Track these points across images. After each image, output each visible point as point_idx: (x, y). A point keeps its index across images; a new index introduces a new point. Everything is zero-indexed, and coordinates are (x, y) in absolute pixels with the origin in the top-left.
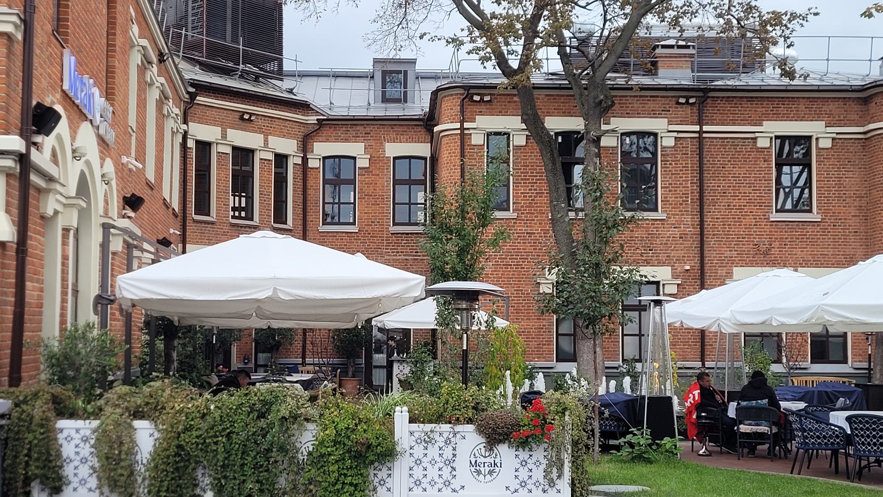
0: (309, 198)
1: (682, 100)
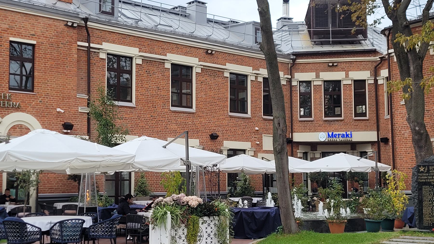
1: (331, 64)
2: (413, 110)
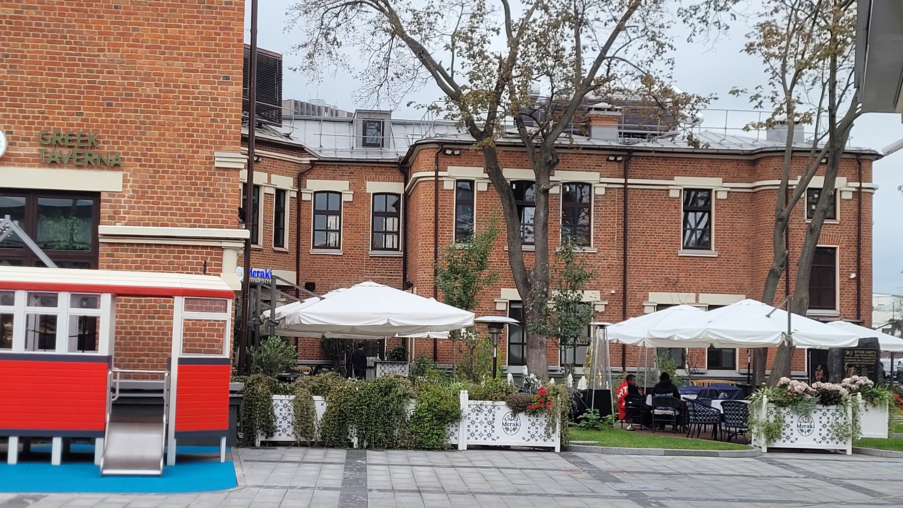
0: (302, 225)
1: (612, 158)
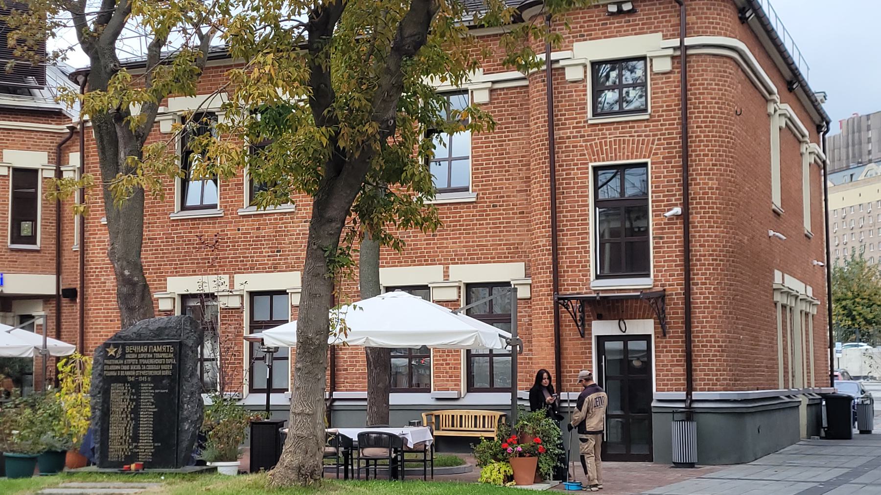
2: (120, 237)
